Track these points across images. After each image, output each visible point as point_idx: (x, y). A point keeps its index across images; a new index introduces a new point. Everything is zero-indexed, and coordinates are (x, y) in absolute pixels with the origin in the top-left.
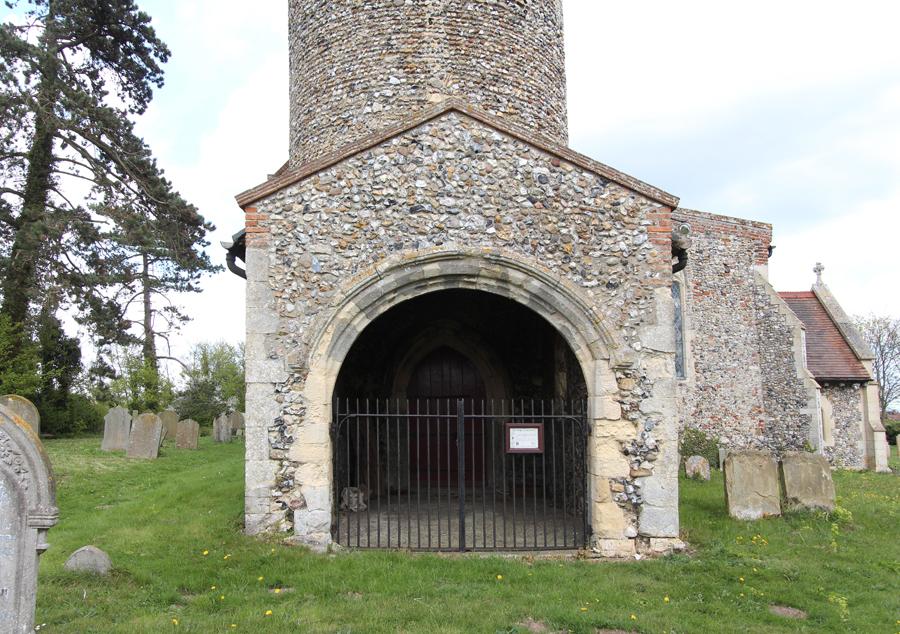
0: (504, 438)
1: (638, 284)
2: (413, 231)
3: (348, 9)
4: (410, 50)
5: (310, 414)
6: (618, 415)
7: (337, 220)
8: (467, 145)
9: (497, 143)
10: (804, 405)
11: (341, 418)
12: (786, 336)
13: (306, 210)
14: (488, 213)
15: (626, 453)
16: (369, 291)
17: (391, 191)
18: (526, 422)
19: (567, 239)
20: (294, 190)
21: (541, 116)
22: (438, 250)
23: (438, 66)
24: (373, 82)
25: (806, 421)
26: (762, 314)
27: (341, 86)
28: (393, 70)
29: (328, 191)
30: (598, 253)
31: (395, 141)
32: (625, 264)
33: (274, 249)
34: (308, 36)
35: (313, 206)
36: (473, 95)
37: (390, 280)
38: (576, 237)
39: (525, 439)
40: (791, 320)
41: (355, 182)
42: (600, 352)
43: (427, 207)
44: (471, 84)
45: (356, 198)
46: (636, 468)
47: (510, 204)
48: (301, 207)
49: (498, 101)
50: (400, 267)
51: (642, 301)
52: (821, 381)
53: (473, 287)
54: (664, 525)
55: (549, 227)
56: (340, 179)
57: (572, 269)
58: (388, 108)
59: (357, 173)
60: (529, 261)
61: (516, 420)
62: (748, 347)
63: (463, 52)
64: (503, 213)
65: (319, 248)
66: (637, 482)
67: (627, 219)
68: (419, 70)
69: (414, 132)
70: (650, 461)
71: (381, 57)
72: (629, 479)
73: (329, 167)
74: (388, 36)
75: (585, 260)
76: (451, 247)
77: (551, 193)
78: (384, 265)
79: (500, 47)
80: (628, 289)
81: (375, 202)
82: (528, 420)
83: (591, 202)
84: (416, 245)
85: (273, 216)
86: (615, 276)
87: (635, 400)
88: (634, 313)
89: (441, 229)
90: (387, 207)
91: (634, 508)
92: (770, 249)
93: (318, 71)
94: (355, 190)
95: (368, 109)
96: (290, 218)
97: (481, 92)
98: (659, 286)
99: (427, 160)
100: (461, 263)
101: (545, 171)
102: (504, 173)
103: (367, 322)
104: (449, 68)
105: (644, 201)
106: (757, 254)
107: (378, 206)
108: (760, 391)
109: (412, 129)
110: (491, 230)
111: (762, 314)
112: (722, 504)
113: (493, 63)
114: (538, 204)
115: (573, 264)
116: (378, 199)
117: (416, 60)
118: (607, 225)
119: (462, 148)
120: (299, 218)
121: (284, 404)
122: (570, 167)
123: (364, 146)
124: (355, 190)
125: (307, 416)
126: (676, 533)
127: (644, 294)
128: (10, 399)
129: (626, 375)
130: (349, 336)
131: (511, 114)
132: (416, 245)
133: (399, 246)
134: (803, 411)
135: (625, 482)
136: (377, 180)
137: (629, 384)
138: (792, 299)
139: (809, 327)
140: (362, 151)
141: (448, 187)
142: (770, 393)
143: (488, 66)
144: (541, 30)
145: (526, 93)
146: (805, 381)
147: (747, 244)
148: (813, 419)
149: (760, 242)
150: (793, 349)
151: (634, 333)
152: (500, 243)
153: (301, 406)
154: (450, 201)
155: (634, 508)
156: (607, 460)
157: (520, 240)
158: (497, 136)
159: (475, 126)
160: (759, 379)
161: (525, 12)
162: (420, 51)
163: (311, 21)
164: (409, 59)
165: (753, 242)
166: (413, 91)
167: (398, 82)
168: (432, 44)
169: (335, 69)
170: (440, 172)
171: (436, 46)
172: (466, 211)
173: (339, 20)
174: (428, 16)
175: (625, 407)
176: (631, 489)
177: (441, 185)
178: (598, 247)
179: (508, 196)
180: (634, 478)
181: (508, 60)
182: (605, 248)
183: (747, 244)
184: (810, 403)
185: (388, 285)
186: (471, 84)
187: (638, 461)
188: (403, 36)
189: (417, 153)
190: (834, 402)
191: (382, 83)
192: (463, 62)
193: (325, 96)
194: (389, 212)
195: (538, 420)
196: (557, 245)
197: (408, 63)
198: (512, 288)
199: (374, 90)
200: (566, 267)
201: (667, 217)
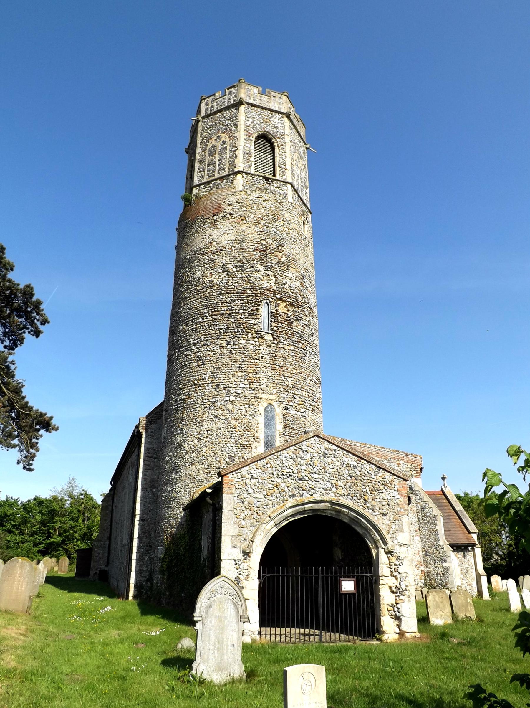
0: (339, 586)
1: (395, 514)
2: (300, 489)
3: (217, 346)
4: (252, 371)
5: (251, 575)
6: (389, 574)
7: (266, 482)
8: (322, 451)
9: (335, 451)
10: (445, 561)
11: (263, 576)
12: (433, 520)
13: (252, 477)
14: (332, 482)
15: (393, 592)
16: (280, 516)
17: (291, 471)
18: (348, 578)
19: (365, 494)
20: (246, 468)
21: (313, 404)
22: (312, 499)
23: (265, 380)
24: (230, 385)
25: (446, 570)
26: (420, 507)
27: (211, 384)
28: (242, 380)
29: (261, 469)
30: (378, 500)
31: (292, 448)
32: (389, 505)
33: (236, 495)
34: (190, 355)
35: (255, 475)
36: (282, 395)
37: (290, 511)
38: (369, 492)
39: (348, 586)
40: (435, 511)
41: (273, 465)
42: (381, 545)
43: (306, 478)
44: (282, 390)
45: (275, 473)
46: (398, 599)
47: (342, 478)
48: (250, 476)
49: (295, 398)
50: (295, 506)
51: (397, 521)
52: (452, 546)
53: (324, 514)
54: (410, 625)
55: (358, 488)
56: (267, 464)
57: (367, 507)
58: (238, 399)
59: (275, 461)
60: (350, 503)
61: (345, 577)
62: (413, 526)
63: (278, 373)
64: (339, 482)
65: (257, 495)
66: (399, 606)
67: (389, 485)
68: (255, 381)
69: (300, 444)
70: (403, 595)
71: (235, 373)
72: (395, 604)
73: (263, 459)
74: (239, 363)
75: (373, 503)
76: (317, 497)
77: (358, 473)
78: (289, 504)
79: (295, 371)
80: (391, 516)
81: (283, 475)
82: (349, 577)
83: (375, 477)
84: (301, 496)
85: (236, 480)
86: (385, 510)
87: (396, 567)
88: (394, 527)
89: (312, 488)
90: (288, 477)
91: (398, 618)
92: (421, 469)
93: (197, 374)
94: (274, 469)
95: (227, 399)
96: (244, 481)
97: (286, 393)
98: (404, 515)
99: (306, 457)
100: (322, 504)
101: (356, 464)
102: (339, 464)
103: (277, 530)
104: (271, 381)
105: (396, 477)
106: (415, 472)
107: (284, 477)
108: (421, 552)
109: (299, 443)
110: (334, 489)
111: (420, 507)
112: (193, 649)
113: (292, 379)
114: (353, 478)
115: (368, 505)
116: (284, 474)
117: (255, 376)
118: (381, 487)
119: (320, 452)
120: (248, 481)
121: (239, 570)
122: (365, 462)
123: (278, 450)
124: (274, 469)
125: (251, 576)
126: (416, 630)
127: (397, 518)
128: (20, 560)
129: (392, 555)
130: (269, 536)
131: (300, 404)
132: (301, 496)
133: (294, 496)
134: (444, 564)
135: (393, 606)
136: (284, 465)
137: (393, 559)
138: (432, 495)
139: (446, 517)
140: (277, 452)
141: (315, 469)
142: (426, 554)
143: (290, 381)
144: (312, 361)
145: (307, 393)
146: (444, 546)
147: (410, 466)
148: (450, 569)
149: (416, 465)
150: (437, 527)
151: (394, 536)
152: (338, 495)
153: (247, 571)
154: (316, 476)
155: (398, 618)
156: (386, 597)
157: (346, 494)
158: (334, 447)
159: (326, 443)
160: (420, 545)
161: (306, 353)
162: (257, 372)
163: (193, 348)
164: (251, 375)
165: (413, 465)
166: (252, 392)
167: (245, 386)
168: (262, 369)
169: (208, 375)
170: (311, 463)
171: (264, 369)
172: (323, 480)
173: (212, 351)
174: (261, 355)
175: (392, 570)
176: (396, 609)
177: (312, 468)
178: (378, 497)
179: (341, 474)
180: (397, 604)
181: (299, 377)
182: (381, 497)
183: (410, 466)
184: (448, 559)
185: (289, 514)
186: (282, 390)
187: (399, 596)
188: (248, 363)
189: (301, 453)
190: (459, 558)
191: (236, 386)
192: (278, 378)
193: (200, 388)
194: (289, 479)
195: (353, 577)
196: (362, 497)
197: (250, 377)
198: (342, 515)
199: (231, 389)
200: (365, 506)
201: (405, 484)
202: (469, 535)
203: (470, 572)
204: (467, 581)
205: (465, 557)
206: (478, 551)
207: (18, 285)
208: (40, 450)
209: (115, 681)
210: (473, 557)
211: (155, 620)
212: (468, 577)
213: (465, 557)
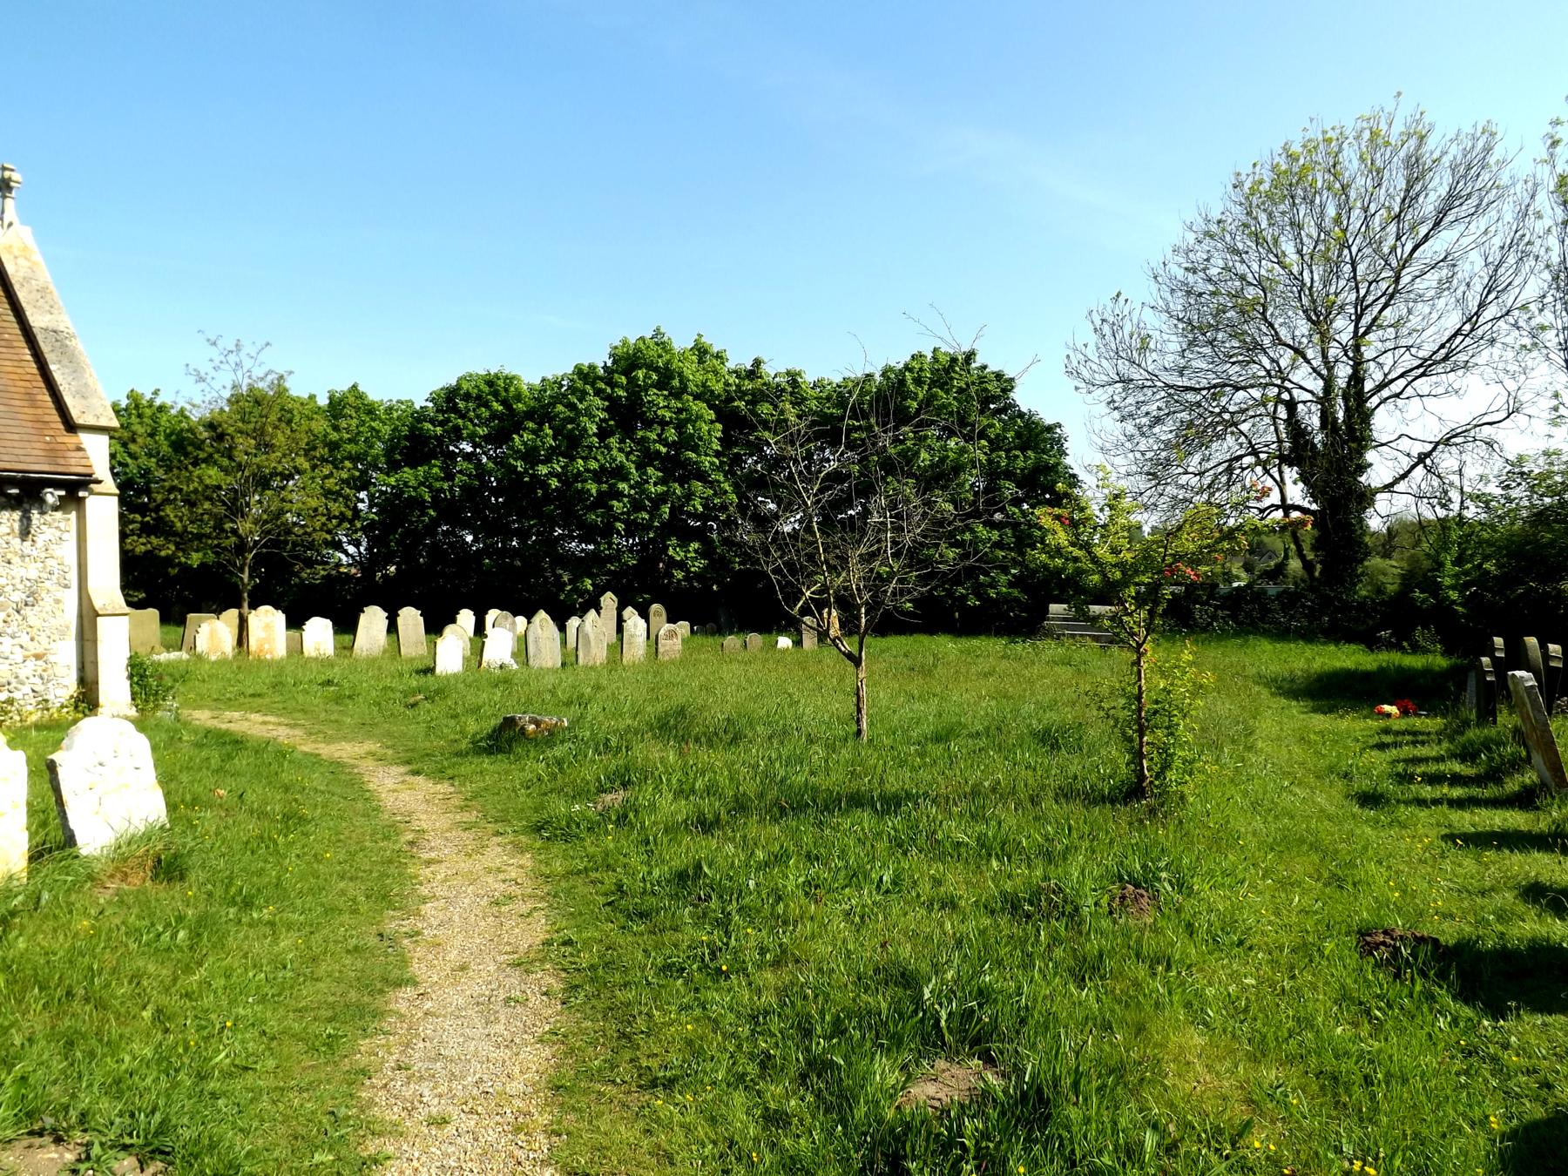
104: (749, 937)
202: (70, 440)
203: (47, 603)
204: (25, 639)
205: (25, 533)
206: (103, 510)
207: (312, 397)
208: (1065, 377)
209: (607, 833)
210: (72, 537)
211: (486, 1099)
212: (32, 620)
213: (25, 533)
